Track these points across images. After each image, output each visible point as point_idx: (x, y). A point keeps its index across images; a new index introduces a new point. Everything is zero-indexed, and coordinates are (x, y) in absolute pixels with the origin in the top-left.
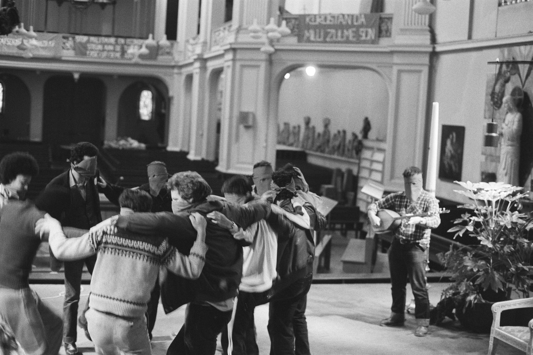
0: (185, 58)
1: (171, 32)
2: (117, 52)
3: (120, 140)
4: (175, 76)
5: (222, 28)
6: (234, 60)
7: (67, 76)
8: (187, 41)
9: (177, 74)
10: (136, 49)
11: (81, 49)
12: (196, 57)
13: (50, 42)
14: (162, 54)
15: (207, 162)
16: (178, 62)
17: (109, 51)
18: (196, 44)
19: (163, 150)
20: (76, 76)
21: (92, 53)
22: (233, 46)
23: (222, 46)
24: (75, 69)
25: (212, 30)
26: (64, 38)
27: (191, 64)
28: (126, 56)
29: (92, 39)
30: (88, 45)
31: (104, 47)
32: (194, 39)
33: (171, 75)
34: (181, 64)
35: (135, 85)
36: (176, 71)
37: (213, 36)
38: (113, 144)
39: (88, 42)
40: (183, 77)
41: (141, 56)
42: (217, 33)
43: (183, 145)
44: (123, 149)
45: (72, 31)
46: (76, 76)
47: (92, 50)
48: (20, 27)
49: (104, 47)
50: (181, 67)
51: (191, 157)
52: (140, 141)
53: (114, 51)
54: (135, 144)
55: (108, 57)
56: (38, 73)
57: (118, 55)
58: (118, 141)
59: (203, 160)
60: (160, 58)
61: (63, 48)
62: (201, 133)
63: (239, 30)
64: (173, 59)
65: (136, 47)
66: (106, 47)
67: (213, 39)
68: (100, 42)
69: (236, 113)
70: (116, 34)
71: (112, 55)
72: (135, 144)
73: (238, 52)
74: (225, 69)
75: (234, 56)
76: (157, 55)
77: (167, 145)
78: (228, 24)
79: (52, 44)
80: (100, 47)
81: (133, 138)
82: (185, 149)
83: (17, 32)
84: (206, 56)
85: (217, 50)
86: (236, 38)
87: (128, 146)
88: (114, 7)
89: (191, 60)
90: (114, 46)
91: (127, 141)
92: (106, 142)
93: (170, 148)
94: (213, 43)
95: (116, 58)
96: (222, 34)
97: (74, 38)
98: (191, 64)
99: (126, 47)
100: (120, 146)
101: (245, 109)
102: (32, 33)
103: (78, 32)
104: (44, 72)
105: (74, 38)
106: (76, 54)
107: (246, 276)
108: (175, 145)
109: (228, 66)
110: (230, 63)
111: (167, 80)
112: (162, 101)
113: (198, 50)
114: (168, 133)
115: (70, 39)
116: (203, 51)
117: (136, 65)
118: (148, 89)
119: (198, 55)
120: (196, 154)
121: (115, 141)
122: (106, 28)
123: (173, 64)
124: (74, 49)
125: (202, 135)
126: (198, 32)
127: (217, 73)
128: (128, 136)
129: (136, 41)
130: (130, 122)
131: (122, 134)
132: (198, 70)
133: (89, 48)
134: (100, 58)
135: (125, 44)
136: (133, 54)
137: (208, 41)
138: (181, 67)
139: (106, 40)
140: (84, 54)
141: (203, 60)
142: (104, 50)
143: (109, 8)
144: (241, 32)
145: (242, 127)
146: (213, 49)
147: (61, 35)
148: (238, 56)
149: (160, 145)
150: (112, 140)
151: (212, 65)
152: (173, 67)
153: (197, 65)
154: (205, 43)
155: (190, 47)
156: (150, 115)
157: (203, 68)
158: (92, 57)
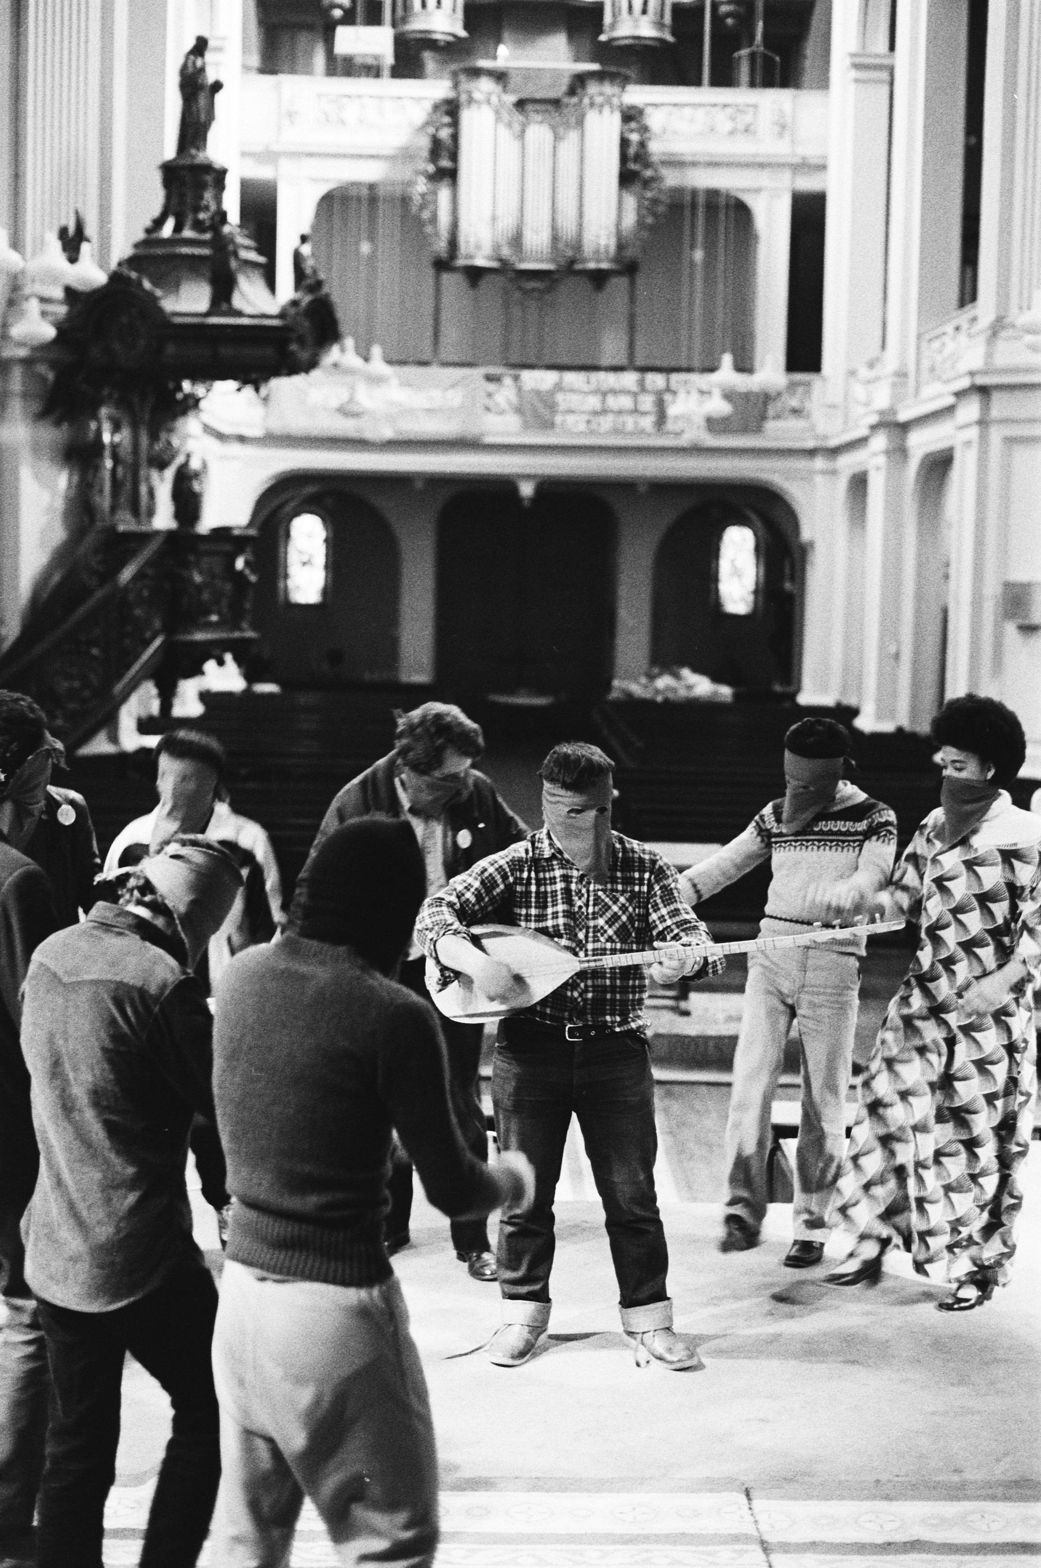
0: (846, 422)
1: (804, 351)
2: (644, 414)
3: (660, 675)
4: (819, 479)
5: (949, 329)
6: (983, 423)
7: (502, 487)
8: (852, 373)
9: (824, 472)
10: (697, 401)
11: (540, 411)
12: (874, 419)
13: (450, 393)
14: (778, 417)
15: (913, 736)
16: (826, 437)
17: (620, 412)
18: (877, 379)
19: (787, 704)
20: (527, 490)
21: (570, 419)
22: (980, 381)
23: (947, 381)
24: (520, 471)
25: (919, 336)
26: (489, 378)
27: (860, 442)
28: (670, 426)
29: (572, 378)
30: (560, 397)
31: (604, 401)
32: (871, 365)
33: (807, 477)
34: (833, 443)
35: (703, 509)
36: (819, 463)
37: (926, 353)
38: (637, 689)
39: (558, 387)
40: (842, 484)
41: (713, 424)
42: (936, 344)
43: (845, 689)
44: (667, 701)
45: (514, 359)
46: (527, 490)
47: (571, 411)
48: (343, 350)
49: (604, 401)
50: (835, 452)
51: (866, 723)
52: (716, 679)
53: (635, 411)
54: (701, 686)
55: (617, 431)
56: (419, 485)
57: (648, 422)
58: (652, 678)
59: (900, 730)
60: (770, 425)
61: (488, 409)
62: (893, 649)
63: (998, 327)
64: (812, 428)
65: (695, 395)
66: (612, 402)
67: (926, 364)
68: (593, 386)
69: (992, 589)
70: (640, 361)
71: (630, 422)
72: (701, 686)
73: (996, 397)
74: (958, 456)
75: (986, 407)
76: (763, 418)
77: (798, 690)
78: (969, 311)
79: (455, 398)
80: (594, 402)
81: (697, 670)
82: (851, 701)
83: (335, 365)
84: (903, 417)
85: (936, 394)
86: (989, 355)
87: (683, 693)
88: (632, 284)
89: (863, 432)
90: (635, 395)
91: (677, 676)
92: (616, 683)
93: (804, 699)
94: (925, 375)
95: (642, 432)
96: (951, 346)
97: (516, 378)
98: (860, 442)
99: (668, 397)
100: (657, 691)
101: (1019, 576)
102: (378, 365)
103: (532, 360)
104: (436, 481)
105: (516, 378)
106: (526, 426)
107: (887, 1125)
108: (824, 688)
109: (968, 443)
110: (974, 433)
111: (796, 493)
112: (784, 557)
113: (882, 399)
114: (801, 654)
115: (508, 381)
116: (897, 398)
117: (697, 450)
118: (742, 521)
119: (881, 413)
120: (879, 717)
121: (643, 680)
122: (612, 346)
123: (810, 444)
124: (519, 410)
125: (897, 656)
126: (883, 346)
127: (939, 465)
128: (683, 664)
129: (695, 378)
130: (689, 624)
131: (665, 657)
132: (882, 460)
133: (562, 406)
134: (592, 432)
135: (668, 389)
136: (687, 418)
137: (912, 368)
138: (835, 452)
139: (610, 379)
140: (548, 425)
141: (899, 428)
142: (604, 412)
143: (619, 285)
144: (1003, 334)
145: (1010, 628)
146: (927, 391)
147: (478, 372)
148: (995, 412)
149: (778, 688)
150: (638, 677)
151: (922, 442)
152: (812, 453)
153: (880, 442)
154: (902, 374)
155: (859, 391)
156: (751, 598)
157: (899, 452)
158: (571, 433)
